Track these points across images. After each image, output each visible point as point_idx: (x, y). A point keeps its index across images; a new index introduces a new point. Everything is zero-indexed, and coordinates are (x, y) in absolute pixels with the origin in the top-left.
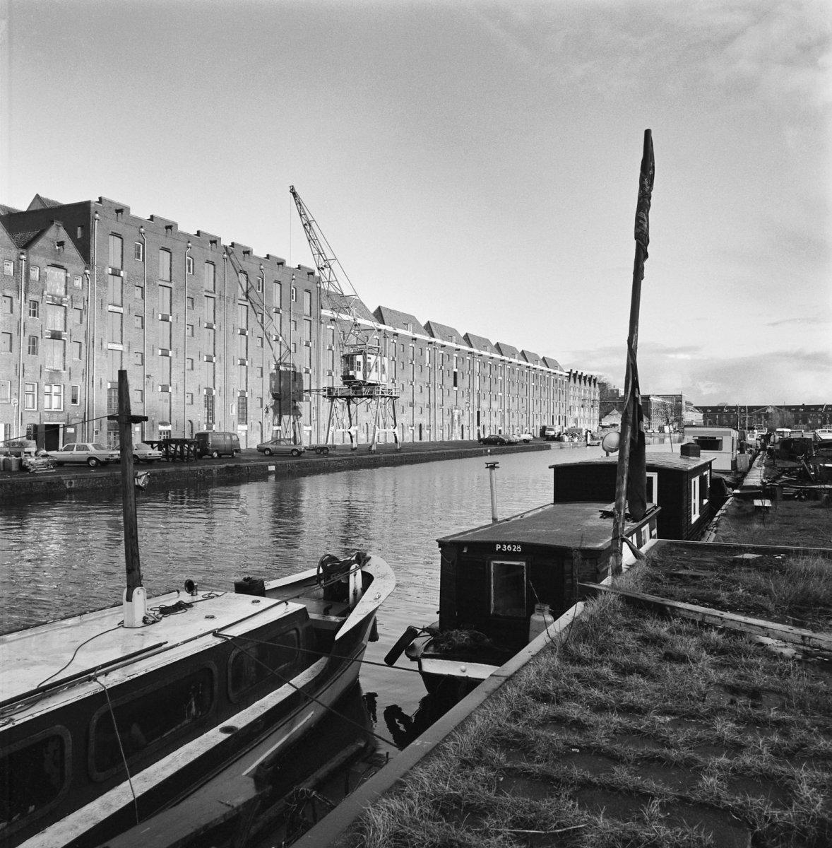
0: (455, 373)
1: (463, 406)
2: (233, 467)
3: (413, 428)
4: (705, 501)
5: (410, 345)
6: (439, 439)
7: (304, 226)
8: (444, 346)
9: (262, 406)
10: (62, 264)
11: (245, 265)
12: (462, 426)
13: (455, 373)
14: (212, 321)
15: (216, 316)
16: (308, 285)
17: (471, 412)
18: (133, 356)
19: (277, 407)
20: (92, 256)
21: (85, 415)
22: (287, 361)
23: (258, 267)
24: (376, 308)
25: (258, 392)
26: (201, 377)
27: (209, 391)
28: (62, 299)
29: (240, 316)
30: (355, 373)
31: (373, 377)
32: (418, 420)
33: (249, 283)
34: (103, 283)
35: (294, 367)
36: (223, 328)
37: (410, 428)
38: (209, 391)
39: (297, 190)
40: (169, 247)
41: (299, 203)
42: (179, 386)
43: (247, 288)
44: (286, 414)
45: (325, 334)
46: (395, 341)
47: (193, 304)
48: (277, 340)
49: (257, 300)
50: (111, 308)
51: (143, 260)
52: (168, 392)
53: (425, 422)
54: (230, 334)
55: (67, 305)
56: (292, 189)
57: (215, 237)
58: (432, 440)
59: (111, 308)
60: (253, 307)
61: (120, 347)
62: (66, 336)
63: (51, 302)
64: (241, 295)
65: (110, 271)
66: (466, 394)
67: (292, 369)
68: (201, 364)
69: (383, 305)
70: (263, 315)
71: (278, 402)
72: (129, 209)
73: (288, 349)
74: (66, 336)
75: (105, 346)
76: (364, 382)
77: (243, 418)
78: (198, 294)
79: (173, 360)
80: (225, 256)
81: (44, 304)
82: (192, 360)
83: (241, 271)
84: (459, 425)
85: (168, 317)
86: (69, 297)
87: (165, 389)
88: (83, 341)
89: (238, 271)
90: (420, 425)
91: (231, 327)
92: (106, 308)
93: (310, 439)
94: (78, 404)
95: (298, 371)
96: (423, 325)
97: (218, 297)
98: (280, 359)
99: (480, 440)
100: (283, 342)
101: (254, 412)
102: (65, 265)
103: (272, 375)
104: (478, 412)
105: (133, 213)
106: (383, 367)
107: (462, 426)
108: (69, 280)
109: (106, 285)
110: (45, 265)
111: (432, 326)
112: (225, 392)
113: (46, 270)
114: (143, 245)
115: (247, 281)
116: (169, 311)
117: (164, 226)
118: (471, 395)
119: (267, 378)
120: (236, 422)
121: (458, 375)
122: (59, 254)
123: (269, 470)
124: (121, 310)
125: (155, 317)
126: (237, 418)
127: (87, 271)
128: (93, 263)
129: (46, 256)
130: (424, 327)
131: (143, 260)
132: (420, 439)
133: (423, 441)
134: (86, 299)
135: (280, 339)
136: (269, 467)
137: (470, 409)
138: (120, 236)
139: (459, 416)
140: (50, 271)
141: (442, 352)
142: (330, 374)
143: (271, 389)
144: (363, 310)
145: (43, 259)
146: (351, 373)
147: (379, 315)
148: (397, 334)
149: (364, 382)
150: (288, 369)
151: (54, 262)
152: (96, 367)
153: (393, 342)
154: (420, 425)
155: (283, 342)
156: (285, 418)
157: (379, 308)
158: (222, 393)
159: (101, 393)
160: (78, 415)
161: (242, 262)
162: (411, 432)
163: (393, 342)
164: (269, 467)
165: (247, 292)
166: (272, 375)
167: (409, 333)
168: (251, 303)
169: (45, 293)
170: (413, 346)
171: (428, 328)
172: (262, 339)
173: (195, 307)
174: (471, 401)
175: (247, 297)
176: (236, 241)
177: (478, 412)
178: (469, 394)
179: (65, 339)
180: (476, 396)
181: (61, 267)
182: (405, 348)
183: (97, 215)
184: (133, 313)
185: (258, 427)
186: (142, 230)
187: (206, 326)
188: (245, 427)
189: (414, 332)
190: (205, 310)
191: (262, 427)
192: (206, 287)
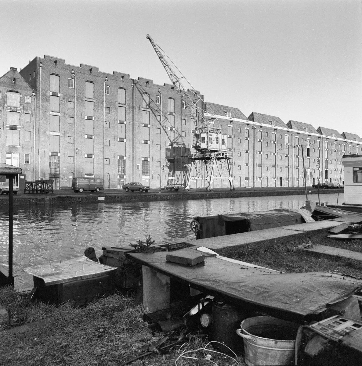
0: (308, 149)
1: (314, 167)
2: (65, 197)
3: (276, 179)
4: (223, 342)
5: (273, 133)
6: (301, 186)
7: (160, 58)
8: (299, 133)
9: (160, 166)
10: (17, 90)
11: (147, 89)
12: (314, 178)
13: (308, 149)
14: (124, 119)
15: (126, 117)
16: (172, 94)
17: (320, 171)
18: (66, 138)
19: (173, 167)
20: (37, 86)
21: (33, 170)
22: (179, 141)
23: (157, 90)
24: (250, 113)
25: (157, 158)
26: (118, 149)
27: (122, 158)
28: (17, 109)
29: (145, 117)
30: (200, 144)
31: (213, 146)
32: (279, 175)
33: (150, 99)
34: (46, 99)
35: (183, 144)
36: (131, 123)
37: (273, 179)
38: (122, 158)
39: (151, 37)
40: (92, 80)
41: (153, 45)
42: (99, 154)
43: (149, 102)
44: (178, 170)
45: (295, 140)
46: (261, 131)
47: (110, 110)
48: (171, 130)
49: (156, 108)
50: (51, 113)
51: (74, 88)
52: (92, 157)
53: (284, 176)
54: (137, 127)
55: (20, 112)
56: (148, 37)
57: (124, 74)
58: (290, 186)
59: (51, 113)
60: (153, 112)
61: (58, 134)
62: (20, 128)
63: (9, 110)
64: (144, 105)
65: (51, 93)
66: (316, 161)
67: (183, 146)
68: (244, 154)
69: (344, 132)
70: (160, 116)
71: (172, 164)
72: (64, 61)
73: (179, 134)
74: (20, 128)
75: (47, 133)
76: (207, 149)
77: (146, 171)
78: (113, 105)
79: (276, 156)
80: (132, 84)
81: (4, 111)
82: (240, 152)
83: (144, 93)
84: (311, 178)
85: (92, 118)
86: (21, 107)
87: (90, 156)
88: (31, 130)
89: (142, 93)
90: (281, 178)
91: (137, 123)
92: (48, 113)
93: (197, 184)
94: (30, 164)
95: (187, 147)
96: (286, 124)
97: (129, 107)
98: (174, 140)
99: (314, 186)
100: (176, 131)
101: (153, 167)
102: (19, 91)
103: (167, 149)
104: (326, 171)
105: (154, 83)
106: (223, 140)
107: (314, 178)
108: (21, 98)
109: (48, 101)
110: (5, 91)
111: (321, 130)
112: (134, 158)
113: (6, 93)
114: (74, 79)
115: (149, 98)
116: (93, 114)
117: (145, 82)
118: (321, 161)
119: (164, 151)
120: (141, 175)
121: (310, 150)
122: (15, 85)
123: (99, 199)
124: (59, 114)
125: (82, 118)
126: (142, 172)
127: (34, 94)
128: (39, 91)
129: (6, 86)
130: (342, 135)
131: (74, 88)
132: (281, 185)
133: (283, 187)
134: (33, 108)
135: (174, 129)
136: (99, 198)
137: (320, 169)
138: (173, 99)
139: (311, 173)
140: (9, 94)
141: (319, 140)
142: (247, 152)
143: (167, 157)
144: (241, 115)
145: (4, 88)
146: (198, 144)
147: (319, 130)
148: (261, 127)
149: (207, 149)
150: (180, 146)
151: (11, 89)
152: (41, 144)
153: (274, 134)
154: (281, 178)
155: (176, 131)
156: (178, 173)
157: (290, 121)
158: (131, 159)
159: (45, 158)
160: (28, 170)
161: (145, 88)
162: (274, 181)
163: (260, 131)
164: (99, 198)
165: (149, 104)
166: (167, 149)
167: (334, 138)
168: (151, 110)
169: (6, 105)
170: (275, 133)
171: (344, 135)
172: (160, 129)
173: (111, 112)
174: (321, 164)
175: (149, 107)
176: (140, 76)
177: (326, 171)
178: (319, 161)
179: (20, 129)
180: (324, 161)
181: (17, 92)
182: (283, 137)
183: (41, 64)
184: (67, 116)
185: (158, 177)
186: (159, 90)
187: (119, 122)
188: (148, 177)
189: (276, 125)
190: (121, 114)
191: (268, 178)
192: (119, 101)
